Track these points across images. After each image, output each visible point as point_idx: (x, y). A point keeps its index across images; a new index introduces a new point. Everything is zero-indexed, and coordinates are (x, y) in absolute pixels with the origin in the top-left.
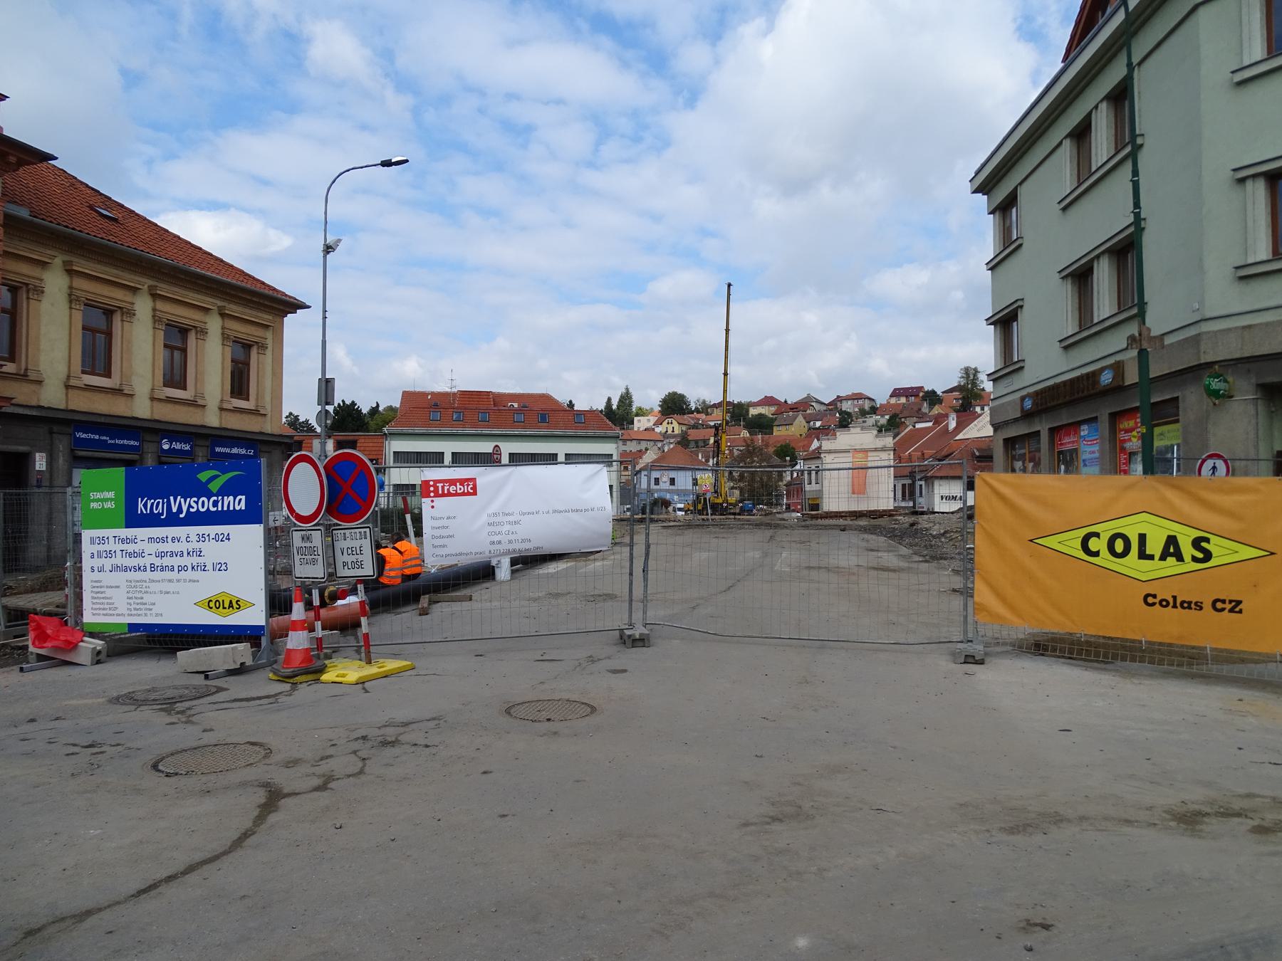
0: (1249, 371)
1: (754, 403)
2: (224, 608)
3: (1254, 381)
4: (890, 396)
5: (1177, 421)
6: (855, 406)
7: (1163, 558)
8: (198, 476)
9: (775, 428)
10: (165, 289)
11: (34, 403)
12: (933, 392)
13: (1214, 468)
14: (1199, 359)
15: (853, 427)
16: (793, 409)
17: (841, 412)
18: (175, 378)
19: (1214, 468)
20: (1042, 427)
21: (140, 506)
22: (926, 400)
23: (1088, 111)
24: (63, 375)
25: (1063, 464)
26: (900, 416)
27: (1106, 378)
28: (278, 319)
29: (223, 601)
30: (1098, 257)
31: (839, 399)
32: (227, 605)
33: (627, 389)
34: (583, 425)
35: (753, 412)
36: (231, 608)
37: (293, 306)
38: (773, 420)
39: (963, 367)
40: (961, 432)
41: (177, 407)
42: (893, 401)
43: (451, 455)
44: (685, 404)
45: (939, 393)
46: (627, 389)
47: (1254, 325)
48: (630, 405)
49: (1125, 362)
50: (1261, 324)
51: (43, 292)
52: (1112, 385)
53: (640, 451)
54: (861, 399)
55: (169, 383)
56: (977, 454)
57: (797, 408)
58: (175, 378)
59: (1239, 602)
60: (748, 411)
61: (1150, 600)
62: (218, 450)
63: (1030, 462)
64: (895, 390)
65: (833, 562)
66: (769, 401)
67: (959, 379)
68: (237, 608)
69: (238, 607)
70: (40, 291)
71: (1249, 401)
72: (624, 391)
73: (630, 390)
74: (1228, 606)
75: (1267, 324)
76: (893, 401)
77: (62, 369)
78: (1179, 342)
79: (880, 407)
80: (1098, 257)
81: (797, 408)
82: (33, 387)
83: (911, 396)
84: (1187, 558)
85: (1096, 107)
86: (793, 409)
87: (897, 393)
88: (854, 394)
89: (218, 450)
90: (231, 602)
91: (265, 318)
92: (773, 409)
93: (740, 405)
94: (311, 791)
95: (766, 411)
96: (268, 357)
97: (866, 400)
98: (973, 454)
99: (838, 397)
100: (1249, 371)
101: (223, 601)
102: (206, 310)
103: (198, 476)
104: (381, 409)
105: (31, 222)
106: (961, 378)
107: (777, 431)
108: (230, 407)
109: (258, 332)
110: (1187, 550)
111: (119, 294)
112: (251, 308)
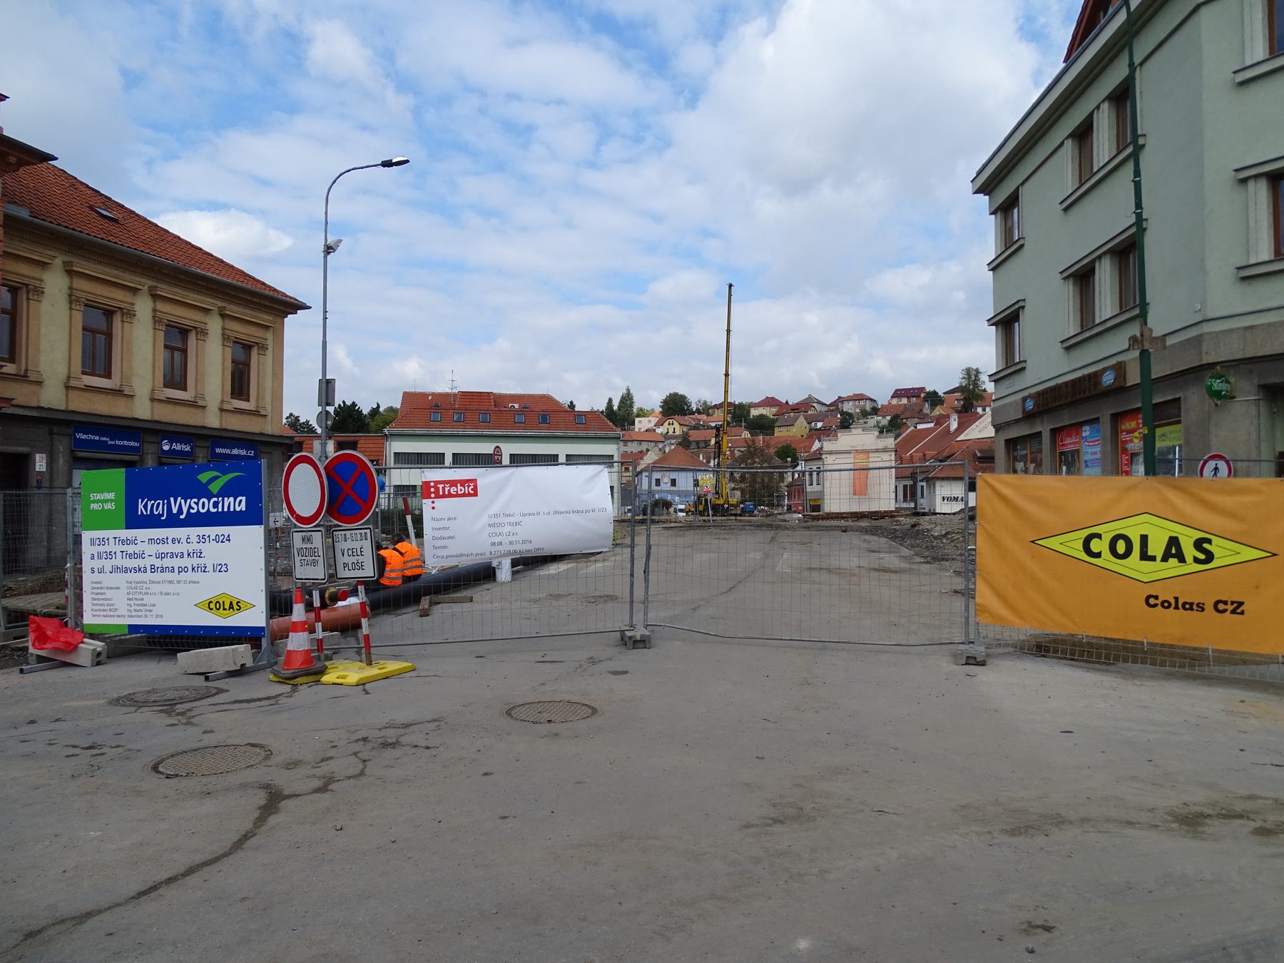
0: (1251, 371)
1: (755, 403)
2: (224, 609)
3: (1255, 381)
4: (892, 397)
5: (1179, 422)
6: (856, 407)
7: (1165, 559)
8: (198, 477)
9: (776, 429)
10: (165, 290)
11: (34, 404)
12: (935, 393)
13: (1216, 469)
14: (1201, 360)
15: (854, 428)
16: (794, 410)
17: (843, 413)
18: (175, 379)
19: (1216, 469)
20: (1044, 427)
21: (141, 507)
22: (928, 401)
23: (1089, 112)
24: (63, 376)
25: (1065, 465)
26: (902, 417)
27: (1108, 379)
28: (278, 320)
29: (224, 602)
30: (1099, 257)
31: (841, 400)
32: (227, 606)
33: (628, 390)
34: (583, 426)
35: (754, 412)
36: (231, 610)
37: (294, 306)
38: (774, 421)
39: (964, 368)
40: (962, 433)
41: (178, 408)
42: (895, 402)
43: (451, 456)
44: (686, 405)
45: (940, 393)
46: (628, 390)
47: (1256, 326)
48: (631, 406)
49: (1127, 363)
50: (1263, 325)
51: (43, 293)
52: (1114, 386)
53: (641, 452)
54: (863, 400)
55: (169, 383)
56: (979, 455)
57: (798, 409)
58: (175, 379)
59: (1241, 604)
60: (749, 412)
61: (1152, 601)
62: (218, 450)
63: (1031, 463)
64: (897, 390)
65: (834, 563)
66: (770, 402)
67: (961, 380)
68: (237, 610)
69: (238, 608)
70: (40, 292)
71: (1250, 402)
72: (625, 392)
73: (631, 391)
74: (1230, 608)
75: (1269, 325)
76: (895, 402)
77: (62, 370)
78: (1181, 343)
79: (881, 408)
80: (1099, 257)
81: (798, 409)
82: (33, 388)
83: (913, 397)
84: (1189, 559)
85: (1098, 107)
86: (794, 410)
87: (898, 394)
88: (855, 395)
89: (218, 450)
90: (231, 603)
91: (265, 318)
92: (774, 410)
93: (741, 406)
94: (311, 793)
95: (767, 412)
96: (269, 358)
97: (868, 401)
98: (975, 455)
99: (840, 397)
100: (1251, 371)
101: (224, 602)
102: (207, 311)
103: (198, 477)
104: (381, 410)
105: (31, 222)
106: (962, 378)
107: (778, 432)
108: (230, 408)
109: (258, 333)
110: (1189, 551)
111: (119, 295)
112: (252, 309)
